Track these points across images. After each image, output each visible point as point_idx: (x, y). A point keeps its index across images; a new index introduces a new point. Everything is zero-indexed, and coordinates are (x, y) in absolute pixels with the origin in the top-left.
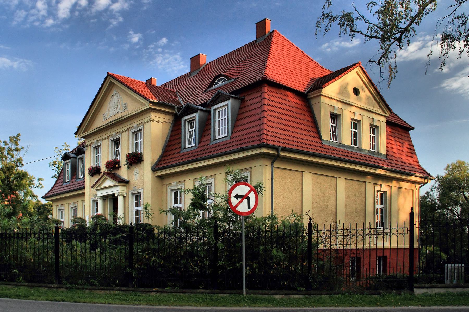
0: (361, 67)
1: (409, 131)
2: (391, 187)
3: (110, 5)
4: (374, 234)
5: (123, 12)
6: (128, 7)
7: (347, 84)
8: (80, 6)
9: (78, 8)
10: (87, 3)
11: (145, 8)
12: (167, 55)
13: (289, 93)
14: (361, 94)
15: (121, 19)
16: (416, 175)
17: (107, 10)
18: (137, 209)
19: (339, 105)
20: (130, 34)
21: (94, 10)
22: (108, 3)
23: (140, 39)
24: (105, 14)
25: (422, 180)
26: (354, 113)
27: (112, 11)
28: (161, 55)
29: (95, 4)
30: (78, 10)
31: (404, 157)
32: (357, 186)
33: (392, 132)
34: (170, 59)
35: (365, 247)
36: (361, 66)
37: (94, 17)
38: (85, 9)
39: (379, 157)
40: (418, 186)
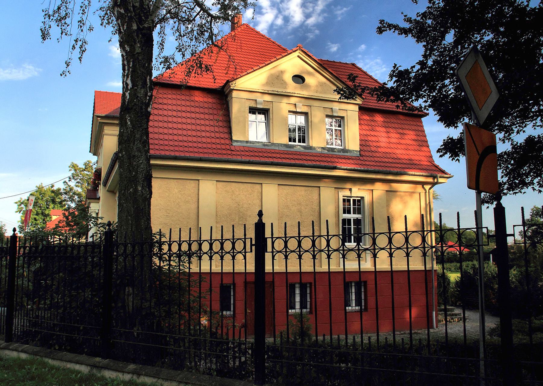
0: (302, 51)
1: (422, 119)
2: (372, 190)
3: (305, 21)
4: (321, 251)
5: (317, 26)
6: (323, 20)
7: (282, 72)
8: (277, 25)
9: (275, 27)
10: (283, 22)
11: (339, 19)
12: (367, 61)
13: (197, 93)
14: (309, 80)
15: (317, 32)
16: (411, 173)
17: (302, 25)
18: (347, 216)
19: (268, 98)
20: (328, 45)
21: (290, 28)
22: (303, 20)
23: (338, 49)
24: (301, 30)
25: (430, 180)
26: (295, 105)
27: (307, 26)
28: (362, 61)
29: (291, 22)
30: (276, 30)
31: (398, 152)
32: (303, 193)
33: (384, 122)
34: (371, 64)
35: (318, 269)
36: (303, 49)
37: (290, 34)
38: (281, 28)
39: (346, 154)
40: (427, 187)
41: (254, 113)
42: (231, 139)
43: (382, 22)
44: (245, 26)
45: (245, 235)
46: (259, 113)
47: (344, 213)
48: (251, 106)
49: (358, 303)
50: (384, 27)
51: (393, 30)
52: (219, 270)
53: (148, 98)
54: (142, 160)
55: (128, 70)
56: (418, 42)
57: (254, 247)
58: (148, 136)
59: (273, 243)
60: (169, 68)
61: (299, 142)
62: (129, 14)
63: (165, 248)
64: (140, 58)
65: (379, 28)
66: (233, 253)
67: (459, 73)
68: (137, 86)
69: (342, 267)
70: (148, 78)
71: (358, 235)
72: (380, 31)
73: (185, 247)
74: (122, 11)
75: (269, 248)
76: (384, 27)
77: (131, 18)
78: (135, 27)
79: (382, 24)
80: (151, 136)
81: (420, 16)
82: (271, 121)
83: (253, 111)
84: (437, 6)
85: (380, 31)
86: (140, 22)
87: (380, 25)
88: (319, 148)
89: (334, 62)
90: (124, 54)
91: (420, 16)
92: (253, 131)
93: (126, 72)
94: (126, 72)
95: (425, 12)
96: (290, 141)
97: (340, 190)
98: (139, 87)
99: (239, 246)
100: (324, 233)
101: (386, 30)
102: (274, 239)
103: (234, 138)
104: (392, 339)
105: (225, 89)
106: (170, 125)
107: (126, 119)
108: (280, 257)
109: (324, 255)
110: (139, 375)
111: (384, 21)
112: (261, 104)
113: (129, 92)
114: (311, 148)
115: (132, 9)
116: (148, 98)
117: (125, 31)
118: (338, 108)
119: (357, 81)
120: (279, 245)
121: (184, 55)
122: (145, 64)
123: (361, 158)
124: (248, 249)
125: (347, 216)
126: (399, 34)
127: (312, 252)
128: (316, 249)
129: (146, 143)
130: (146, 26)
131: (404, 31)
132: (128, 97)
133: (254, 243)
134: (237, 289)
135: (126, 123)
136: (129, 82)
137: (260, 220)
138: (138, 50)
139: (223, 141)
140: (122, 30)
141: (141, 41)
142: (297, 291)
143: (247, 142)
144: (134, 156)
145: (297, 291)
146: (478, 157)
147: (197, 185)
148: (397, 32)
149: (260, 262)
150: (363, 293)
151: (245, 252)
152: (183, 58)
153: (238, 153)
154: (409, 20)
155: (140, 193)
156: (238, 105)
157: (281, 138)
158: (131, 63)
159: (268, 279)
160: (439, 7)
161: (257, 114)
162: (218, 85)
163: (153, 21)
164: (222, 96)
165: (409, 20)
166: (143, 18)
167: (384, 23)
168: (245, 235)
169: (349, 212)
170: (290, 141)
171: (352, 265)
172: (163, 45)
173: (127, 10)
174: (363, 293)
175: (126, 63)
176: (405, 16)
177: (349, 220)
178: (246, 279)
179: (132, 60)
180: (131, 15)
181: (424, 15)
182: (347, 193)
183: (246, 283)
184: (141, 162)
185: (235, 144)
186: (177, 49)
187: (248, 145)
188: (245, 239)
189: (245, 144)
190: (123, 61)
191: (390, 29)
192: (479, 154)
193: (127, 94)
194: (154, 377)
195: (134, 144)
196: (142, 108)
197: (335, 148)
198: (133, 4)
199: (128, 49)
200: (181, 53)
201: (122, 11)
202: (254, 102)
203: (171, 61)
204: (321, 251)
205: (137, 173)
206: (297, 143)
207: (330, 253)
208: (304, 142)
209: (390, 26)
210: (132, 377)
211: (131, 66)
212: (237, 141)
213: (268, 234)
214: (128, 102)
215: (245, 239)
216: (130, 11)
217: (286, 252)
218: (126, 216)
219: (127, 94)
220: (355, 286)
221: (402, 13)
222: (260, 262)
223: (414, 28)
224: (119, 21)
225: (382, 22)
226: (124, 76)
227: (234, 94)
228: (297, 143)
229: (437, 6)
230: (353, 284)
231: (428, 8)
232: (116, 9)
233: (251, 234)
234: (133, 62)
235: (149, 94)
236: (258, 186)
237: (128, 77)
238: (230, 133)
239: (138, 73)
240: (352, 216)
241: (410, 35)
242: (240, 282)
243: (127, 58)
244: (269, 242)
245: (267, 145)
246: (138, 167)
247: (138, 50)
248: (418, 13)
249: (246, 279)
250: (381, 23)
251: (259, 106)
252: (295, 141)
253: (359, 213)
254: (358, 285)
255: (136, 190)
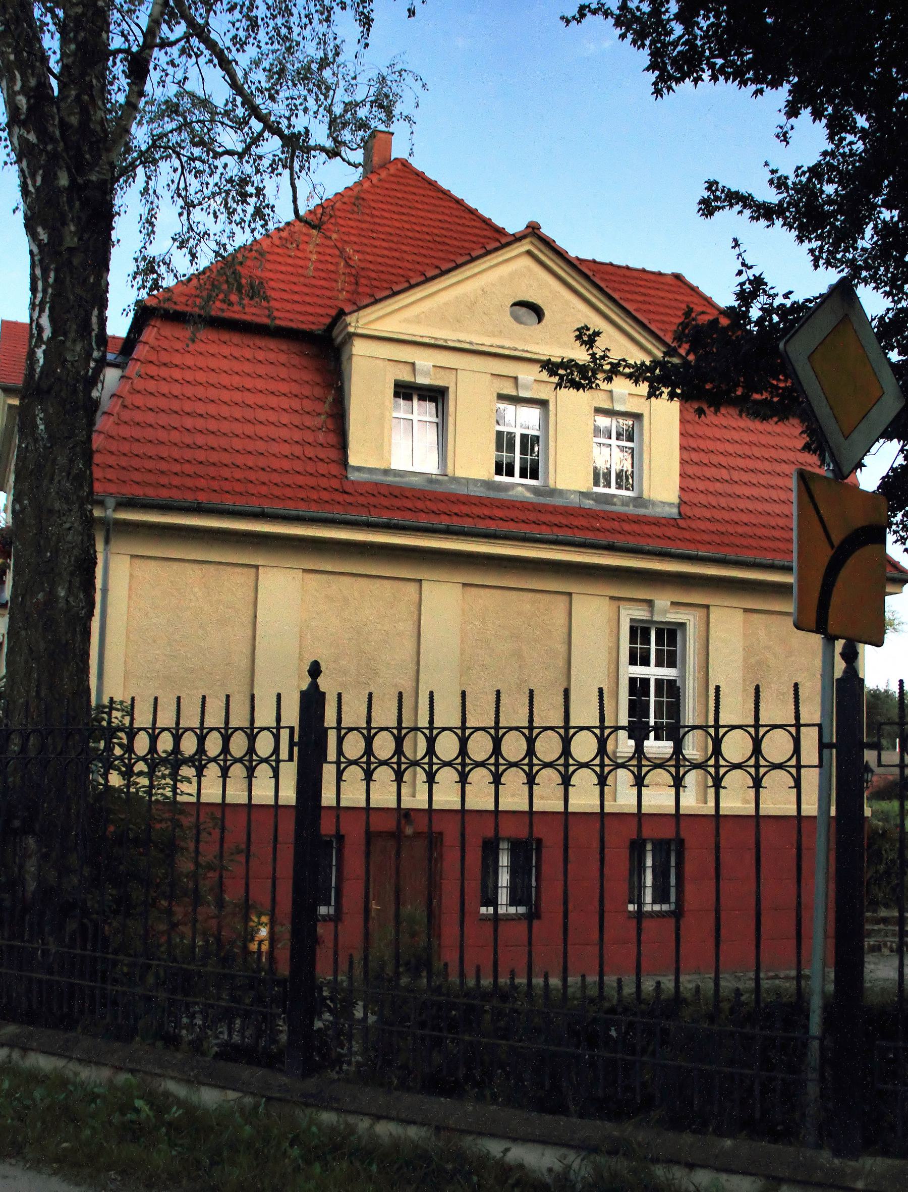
4: (415, 763)
18: (639, 671)
41: (408, 397)
42: (344, 462)
43: (711, 185)
44: (400, 165)
45: (278, 720)
46: (421, 398)
47: (633, 661)
48: (400, 378)
49: (661, 896)
50: (717, 199)
51: (738, 208)
52: (243, 799)
53: (92, 364)
54: (72, 520)
55: (45, 291)
56: (802, 241)
57: (296, 749)
58: (89, 462)
59: (340, 740)
60: (156, 285)
61: (523, 475)
62: (49, 147)
63: (142, 744)
64: (76, 261)
65: (704, 201)
66: (251, 761)
67: (788, 349)
68: (65, 334)
69: (711, 803)
70: (95, 312)
71: (640, 719)
72: (708, 208)
73: (165, 743)
74: (32, 137)
75: (332, 755)
76: (717, 199)
77: (54, 157)
78: (63, 180)
79: (713, 192)
80: (97, 458)
81: (804, 173)
82: (451, 420)
83: (405, 391)
84: (847, 150)
85: (708, 208)
86: (78, 167)
87: (706, 194)
88: (575, 492)
89: (627, 268)
90: (36, 250)
91: (804, 173)
92: (396, 444)
93: (40, 295)
94: (40, 295)
95: (819, 164)
96: (499, 471)
97: (623, 605)
98: (72, 335)
99: (264, 745)
100: (423, 722)
101: (723, 208)
102: (343, 732)
103: (353, 461)
104: (711, 985)
105: (335, 332)
106: (189, 422)
107: (35, 416)
108: (354, 774)
109: (421, 776)
110: (25, 1050)
111: (717, 183)
112: (426, 373)
113: (44, 347)
114: (553, 492)
115: (57, 133)
116: (92, 364)
117: (37, 189)
118: (627, 392)
119: (601, 344)
120: (354, 747)
121: (194, 256)
122: (88, 278)
123: (682, 523)
124: (284, 754)
125: (639, 671)
126: (752, 218)
127: (426, 767)
128: (403, 760)
129: (83, 479)
130: (94, 178)
131: (765, 212)
132: (41, 361)
133: (296, 739)
134: (347, 852)
135: (36, 426)
136: (45, 321)
137: (314, 686)
138: (71, 241)
139: (322, 468)
140: (31, 188)
141: (79, 218)
142: (504, 860)
143: (387, 472)
144: (51, 511)
145: (504, 860)
146: (830, 553)
147: (251, 582)
148: (747, 213)
149: (309, 784)
150: (673, 871)
151: (278, 761)
152: (191, 262)
153: (361, 500)
154: (780, 183)
155: (62, 604)
156: (369, 372)
157: (474, 464)
158: (52, 275)
159: (327, 827)
160: (852, 154)
161: (415, 401)
162: (315, 323)
163: (112, 166)
164: (325, 352)
165: (780, 183)
166: (88, 156)
167: (717, 189)
168: (278, 720)
169: (646, 662)
170: (499, 471)
171: (659, 798)
172: (152, 224)
173: (42, 134)
174: (673, 871)
175: (38, 272)
176: (773, 172)
177: (645, 682)
178: (368, 824)
179: (52, 266)
180: (55, 149)
181: (815, 172)
182: (641, 614)
183: (370, 837)
184: (67, 525)
185: (353, 476)
186: (174, 240)
187: (390, 479)
188: (278, 728)
189: (379, 478)
190: (33, 267)
191: (731, 206)
192: (832, 546)
193: (40, 353)
194: (60, 1056)
195: (52, 480)
196: (75, 391)
197: (614, 496)
198: (61, 120)
199: (43, 236)
200: (185, 250)
201: (32, 137)
202: (409, 368)
203: (163, 269)
204: (415, 763)
205: (56, 552)
206: (517, 479)
207: (372, 767)
208: (535, 476)
209: (734, 198)
210: (9, 1056)
211: (51, 280)
212: (359, 469)
213: (330, 718)
214: (42, 372)
215: (278, 728)
216: (53, 140)
217: (369, 763)
218: (26, 662)
219: (40, 353)
220: (653, 850)
221: (766, 164)
222: (309, 784)
223: (789, 203)
224: (24, 164)
225: (711, 185)
226: (33, 306)
227: (359, 348)
228: (517, 479)
229: (847, 150)
230: (649, 847)
231: (825, 154)
232: (16, 130)
233: (292, 716)
234: (57, 271)
235: (96, 354)
236: (412, 588)
237: (42, 311)
238: (343, 446)
239: (68, 300)
240: (653, 672)
241: (779, 222)
242: (354, 834)
243: (41, 261)
244: (332, 736)
245: (437, 482)
246: (58, 541)
247: (71, 241)
248: (798, 168)
249: (368, 824)
250: (709, 189)
251: (422, 380)
252: (510, 473)
253: (672, 664)
254: (662, 848)
255: (52, 597)
